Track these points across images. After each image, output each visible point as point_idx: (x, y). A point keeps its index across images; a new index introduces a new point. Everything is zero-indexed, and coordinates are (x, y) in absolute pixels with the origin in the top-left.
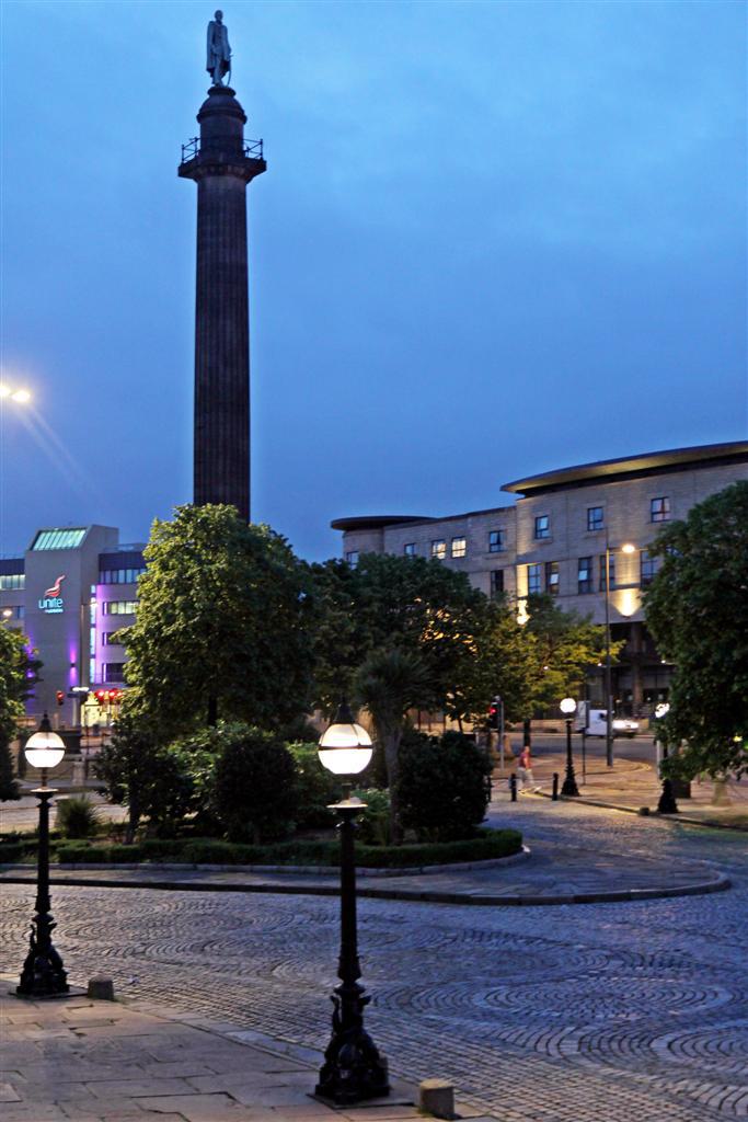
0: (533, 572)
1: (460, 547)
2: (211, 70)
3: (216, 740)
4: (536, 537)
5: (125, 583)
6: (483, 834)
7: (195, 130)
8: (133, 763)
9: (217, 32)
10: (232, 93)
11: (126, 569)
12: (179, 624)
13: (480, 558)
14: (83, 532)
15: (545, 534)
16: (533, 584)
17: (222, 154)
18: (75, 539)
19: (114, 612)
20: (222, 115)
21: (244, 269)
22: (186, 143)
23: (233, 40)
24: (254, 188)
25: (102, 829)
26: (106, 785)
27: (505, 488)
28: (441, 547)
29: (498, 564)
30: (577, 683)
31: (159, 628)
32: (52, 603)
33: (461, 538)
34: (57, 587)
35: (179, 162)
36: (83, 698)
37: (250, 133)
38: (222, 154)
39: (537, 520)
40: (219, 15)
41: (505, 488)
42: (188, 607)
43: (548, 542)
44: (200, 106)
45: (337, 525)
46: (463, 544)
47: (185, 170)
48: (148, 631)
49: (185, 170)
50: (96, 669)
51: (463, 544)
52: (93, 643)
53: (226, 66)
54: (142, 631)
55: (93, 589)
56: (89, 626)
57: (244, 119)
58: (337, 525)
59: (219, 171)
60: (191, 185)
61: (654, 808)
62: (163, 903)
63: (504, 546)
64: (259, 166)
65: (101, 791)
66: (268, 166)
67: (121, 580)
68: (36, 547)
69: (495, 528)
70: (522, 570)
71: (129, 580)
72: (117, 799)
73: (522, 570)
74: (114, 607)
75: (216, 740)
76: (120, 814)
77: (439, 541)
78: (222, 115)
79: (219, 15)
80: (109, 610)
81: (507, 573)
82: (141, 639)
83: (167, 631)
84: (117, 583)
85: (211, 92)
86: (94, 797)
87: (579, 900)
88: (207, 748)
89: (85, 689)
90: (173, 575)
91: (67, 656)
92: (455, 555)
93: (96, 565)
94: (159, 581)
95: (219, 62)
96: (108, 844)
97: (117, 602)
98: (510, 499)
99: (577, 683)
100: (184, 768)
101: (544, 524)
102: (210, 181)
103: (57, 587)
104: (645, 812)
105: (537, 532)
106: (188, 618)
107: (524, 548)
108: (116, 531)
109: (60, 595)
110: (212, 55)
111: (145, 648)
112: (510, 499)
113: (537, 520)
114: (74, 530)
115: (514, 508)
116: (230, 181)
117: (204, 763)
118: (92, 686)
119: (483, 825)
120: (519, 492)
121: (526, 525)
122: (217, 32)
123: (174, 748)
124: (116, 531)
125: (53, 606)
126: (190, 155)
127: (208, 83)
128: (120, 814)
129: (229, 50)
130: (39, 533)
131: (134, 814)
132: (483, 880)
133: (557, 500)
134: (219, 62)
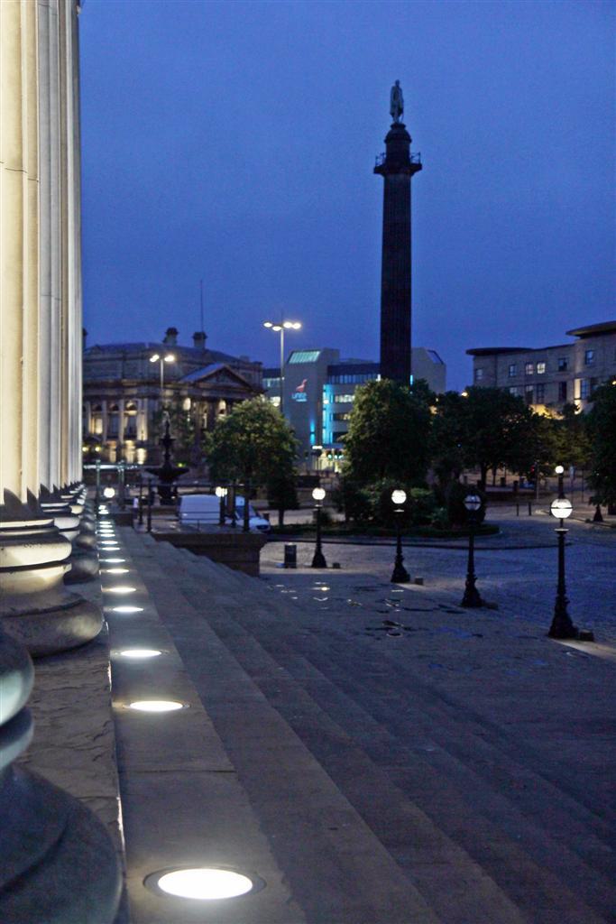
0: (583, 384)
1: (541, 368)
2: (393, 114)
3: (381, 487)
4: (586, 363)
5: (344, 383)
6: (485, 526)
7: (383, 148)
8: (344, 494)
9: (396, 92)
10: (404, 126)
11: (344, 375)
12: (367, 435)
13: (553, 375)
14: (318, 353)
15: (591, 361)
16: (583, 391)
17: (398, 162)
18: (314, 356)
19: (337, 400)
20: (398, 138)
21: (409, 224)
22: (378, 155)
23: (406, 95)
24: (416, 179)
25: (333, 523)
26: (335, 504)
27: (569, 333)
28: (530, 366)
29: (564, 378)
30: (590, 453)
31: (358, 436)
32: (300, 395)
33: (542, 362)
34: (302, 386)
35: (374, 166)
36: (319, 453)
37: (414, 149)
38: (398, 162)
39: (587, 352)
40: (397, 83)
41: (569, 333)
42: (371, 426)
43: (593, 366)
44: (385, 135)
45: (470, 352)
46: (543, 366)
47: (378, 170)
48: (354, 437)
49: (378, 170)
50: (327, 435)
51: (543, 366)
52: (367, 571)
53: (401, 111)
54: (351, 437)
55: (325, 387)
56: (322, 409)
57: (410, 141)
58: (470, 352)
59: (397, 172)
60: (380, 179)
61: (592, 519)
62: (357, 548)
63: (568, 367)
64: (418, 167)
65: (334, 507)
66: (423, 168)
67: (341, 381)
68: (291, 361)
69: (561, 357)
70: (577, 382)
71: (346, 382)
72: (340, 511)
73: (577, 382)
74: (337, 398)
75: (381, 487)
76: (341, 517)
77: (529, 363)
78: (398, 138)
79: (397, 83)
80: (334, 399)
81: (569, 384)
82: (350, 441)
83: (362, 437)
84: (339, 383)
85: (392, 126)
86: (331, 510)
87: (506, 548)
88: (378, 490)
89: (320, 447)
90: (364, 413)
91: (309, 428)
92: (539, 372)
93: (326, 372)
94: (359, 415)
95: (397, 110)
96: (336, 529)
97: (339, 395)
98: (572, 340)
99: (590, 453)
100: (368, 498)
101: (590, 355)
102: (391, 177)
103: (302, 386)
104: (588, 521)
105: (586, 360)
106: (371, 433)
107: (578, 369)
108: (338, 351)
109: (305, 390)
110: (393, 106)
111: (352, 444)
112: (572, 340)
113: (587, 352)
114: (313, 351)
115: (573, 345)
116: (401, 176)
117: (375, 496)
118: (325, 446)
119: (484, 523)
120: (578, 335)
121: (580, 356)
122: (396, 92)
123: (364, 491)
124: (338, 351)
125: (301, 398)
126: (380, 162)
127: (391, 121)
128: (341, 517)
129: (403, 101)
130: (292, 353)
131: (347, 517)
132: (457, 540)
133: (598, 342)
134: (397, 110)
